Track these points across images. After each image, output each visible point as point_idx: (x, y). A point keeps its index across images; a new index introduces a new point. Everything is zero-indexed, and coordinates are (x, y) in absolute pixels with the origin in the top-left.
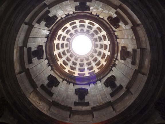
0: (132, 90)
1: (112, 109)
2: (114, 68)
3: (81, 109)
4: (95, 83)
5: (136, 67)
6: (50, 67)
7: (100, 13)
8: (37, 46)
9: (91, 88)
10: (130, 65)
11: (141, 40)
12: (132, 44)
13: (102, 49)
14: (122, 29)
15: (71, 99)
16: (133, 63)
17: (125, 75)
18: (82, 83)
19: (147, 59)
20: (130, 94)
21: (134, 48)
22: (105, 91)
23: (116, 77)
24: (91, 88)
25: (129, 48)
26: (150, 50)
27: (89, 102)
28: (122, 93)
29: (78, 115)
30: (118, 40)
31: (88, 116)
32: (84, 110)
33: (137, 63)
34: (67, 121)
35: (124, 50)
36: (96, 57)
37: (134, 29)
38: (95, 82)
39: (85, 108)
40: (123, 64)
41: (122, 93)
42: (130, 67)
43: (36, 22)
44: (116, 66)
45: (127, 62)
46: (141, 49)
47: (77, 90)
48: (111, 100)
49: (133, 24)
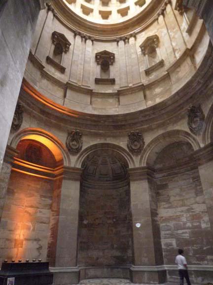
0: (123, 99)
2: (121, 43)
4: (84, 39)
6: (88, 41)
7: (164, 212)
8: (96, 63)
9: (75, 43)
10: (143, 69)
11: (178, 70)
12: (167, 54)
14: (179, 22)
16: (148, 72)
17: (127, 72)
18: (65, 22)
19: (162, 89)
20: (117, 99)
24: (75, 43)
25: (161, 50)
28: (109, 90)
29: (48, 80)
30: (161, 17)
31: (59, 89)
32: (56, 77)
33: (150, 78)
34: (36, 85)
35: (154, 42)
37: (190, 53)
38: (84, 37)
39: (57, 75)
41: (109, 90)
42: (141, 71)
44: (127, 45)
45: (142, 58)
46: (168, 73)
47: (56, 35)
49: (192, 48)
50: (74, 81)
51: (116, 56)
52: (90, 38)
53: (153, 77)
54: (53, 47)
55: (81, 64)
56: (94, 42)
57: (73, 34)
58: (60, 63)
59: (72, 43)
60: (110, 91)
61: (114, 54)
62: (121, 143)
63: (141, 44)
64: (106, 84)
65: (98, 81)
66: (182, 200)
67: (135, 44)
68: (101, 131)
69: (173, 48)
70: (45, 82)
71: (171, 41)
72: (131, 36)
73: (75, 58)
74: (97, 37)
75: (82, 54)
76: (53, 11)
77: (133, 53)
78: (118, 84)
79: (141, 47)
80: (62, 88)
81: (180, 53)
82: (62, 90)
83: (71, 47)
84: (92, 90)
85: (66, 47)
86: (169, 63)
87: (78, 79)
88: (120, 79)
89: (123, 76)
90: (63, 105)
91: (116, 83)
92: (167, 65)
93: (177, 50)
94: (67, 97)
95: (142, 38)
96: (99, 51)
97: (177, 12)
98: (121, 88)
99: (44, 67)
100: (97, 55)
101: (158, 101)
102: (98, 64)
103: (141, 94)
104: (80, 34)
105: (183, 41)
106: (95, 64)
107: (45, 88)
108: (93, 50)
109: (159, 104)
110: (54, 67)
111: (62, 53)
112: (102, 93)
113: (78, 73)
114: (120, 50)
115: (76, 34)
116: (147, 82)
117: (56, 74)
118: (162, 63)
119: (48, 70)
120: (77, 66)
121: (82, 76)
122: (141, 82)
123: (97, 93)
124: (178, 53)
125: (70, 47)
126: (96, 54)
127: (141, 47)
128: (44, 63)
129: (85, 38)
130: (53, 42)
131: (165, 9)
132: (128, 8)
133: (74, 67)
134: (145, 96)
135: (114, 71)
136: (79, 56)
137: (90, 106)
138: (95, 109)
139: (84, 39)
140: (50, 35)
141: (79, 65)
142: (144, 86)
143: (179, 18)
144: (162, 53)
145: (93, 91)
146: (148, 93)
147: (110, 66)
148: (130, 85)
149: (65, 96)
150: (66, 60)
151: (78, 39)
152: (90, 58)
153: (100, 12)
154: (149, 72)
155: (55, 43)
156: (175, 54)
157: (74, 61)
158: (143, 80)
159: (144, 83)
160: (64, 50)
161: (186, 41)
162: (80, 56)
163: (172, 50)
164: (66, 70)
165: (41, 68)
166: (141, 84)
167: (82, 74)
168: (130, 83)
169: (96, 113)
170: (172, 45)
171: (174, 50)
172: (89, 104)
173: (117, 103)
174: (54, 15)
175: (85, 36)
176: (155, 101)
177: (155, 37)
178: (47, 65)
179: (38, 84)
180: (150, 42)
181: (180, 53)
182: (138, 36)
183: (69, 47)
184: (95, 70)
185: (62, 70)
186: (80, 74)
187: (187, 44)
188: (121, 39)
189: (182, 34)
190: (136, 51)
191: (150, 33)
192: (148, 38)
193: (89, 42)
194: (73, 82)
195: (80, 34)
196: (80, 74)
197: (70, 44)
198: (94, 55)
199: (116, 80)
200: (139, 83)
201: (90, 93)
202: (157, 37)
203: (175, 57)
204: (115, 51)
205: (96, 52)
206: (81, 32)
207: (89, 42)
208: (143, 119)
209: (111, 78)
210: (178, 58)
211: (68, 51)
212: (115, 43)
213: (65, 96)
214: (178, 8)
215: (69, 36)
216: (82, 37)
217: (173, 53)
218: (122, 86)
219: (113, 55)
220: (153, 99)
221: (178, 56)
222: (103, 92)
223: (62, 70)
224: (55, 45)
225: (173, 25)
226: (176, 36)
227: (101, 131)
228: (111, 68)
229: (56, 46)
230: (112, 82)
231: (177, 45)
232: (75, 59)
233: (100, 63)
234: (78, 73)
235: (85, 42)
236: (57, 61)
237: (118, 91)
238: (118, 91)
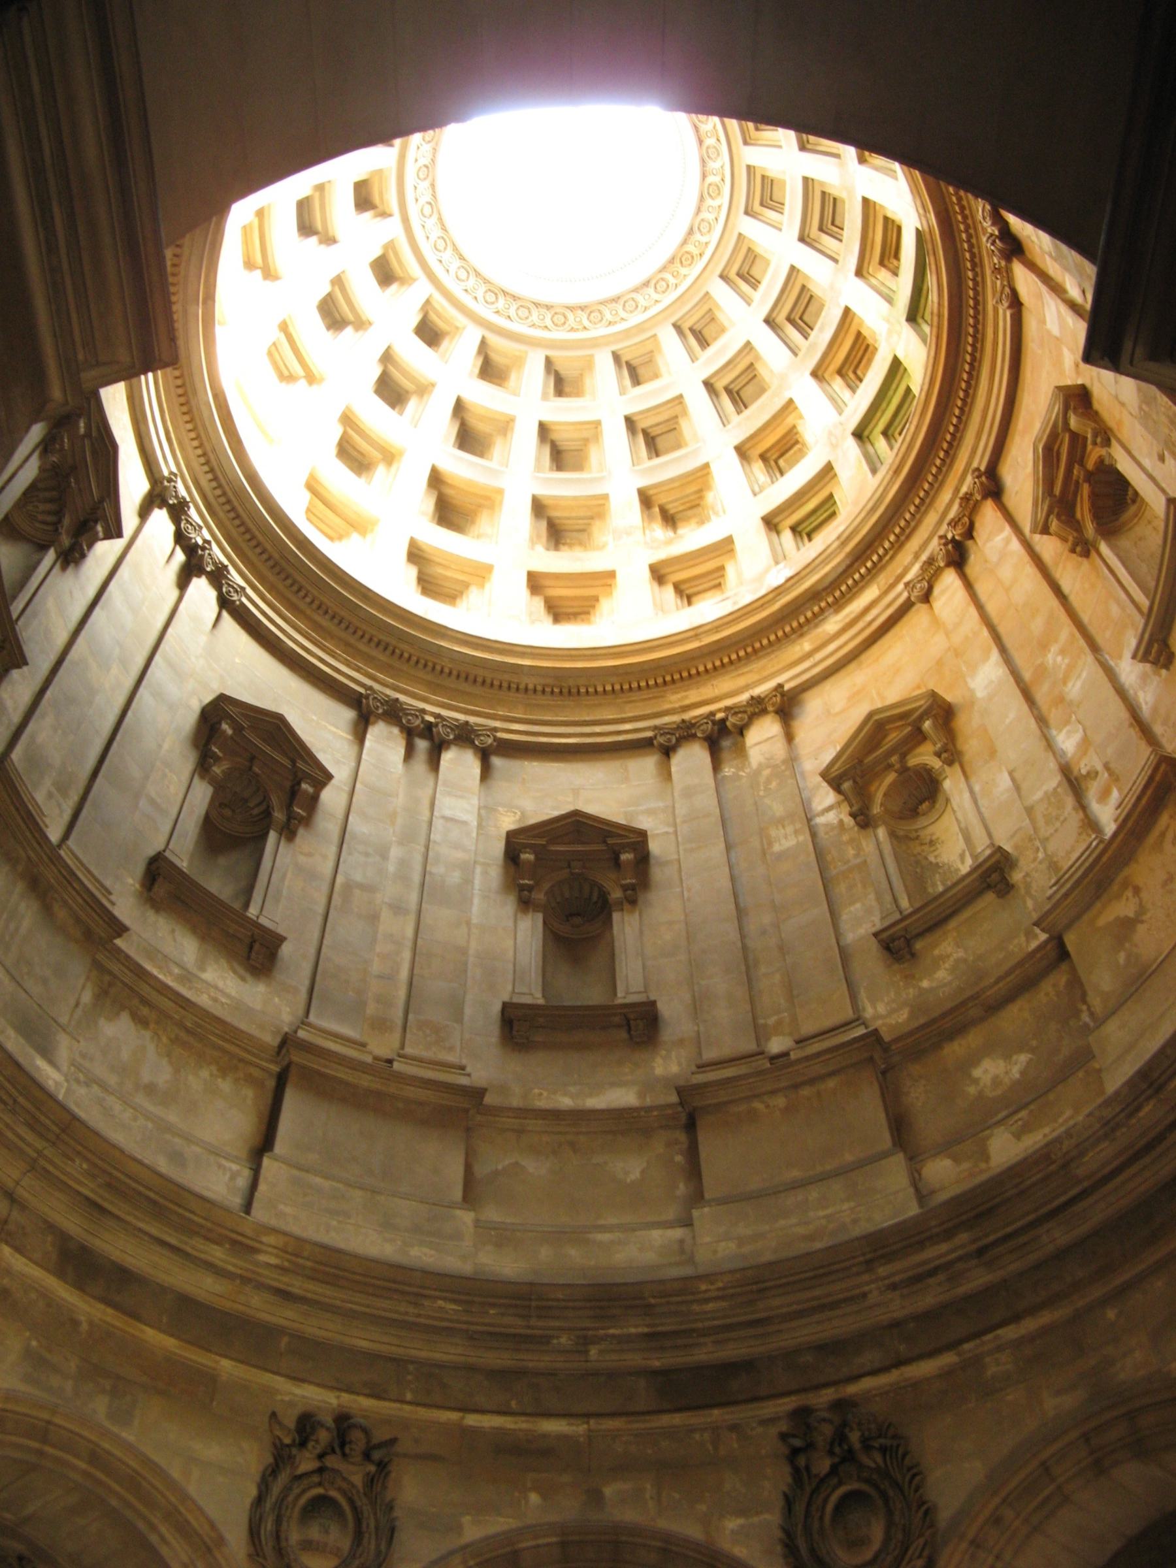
1: (455, 1170)
2: (692, 759)
3: (187, 977)
4: (422, 745)
5: (887, 1008)
6: (449, 757)
10: (862, 919)
12: (1029, 811)
13: (724, 420)
15: (143, 803)
16: (900, 945)
19: (1047, 1130)
21: (1007, 847)
22: (475, 921)
23: (657, 874)
26: (1117, 1093)
27: (281, 939)
29: (141, 1022)
30: (950, 580)
31: (225, 1085)
32: (203, 1000)
33: (925, 984)
36: (597, 424)
38: (428, 731)
39: (220, 985)
40: (805, 837)
42: (850, 937)
43: (802, 454)
48: (484, 1064)
50: (332, 1026)
51: (654, 846)
52: (464, 736)
53: (947, 964)
54: (202, 794)
55: (398, 909)
56: (496, 761)
57: (348, 715)
58: (247, 905)
59: (340, 772)
60: (623, 1097)
61: (643, 834)
62: (732, 1524)
63: (828, 756)
64: (582, 1047)
65: (519, 1026)
66: (1151, 1084)
67: (792, 760)
68: (552, 1426)
69: (1066, 771)
70: (119, 1031)
71: (1042, 721)
72: (757, 708)
73: (355, 868)
74: (516, 731)
75: (406, 838)
76: (217, 577)
77: (780, 822)
78: (681, 1042)
79: (834, 779)
80: (251, 1080)
81: (1115, 795)
82: (249, 1093)
83: (332, 798)
84: (480, 1093)
85: (293, 793)
86: (1053, 866)
87: (371, 1009)
88: (698, 1006)
89: (720, 983)
90: (248, 1207)
91: (667, 1034)
92: (1036, 880)
93: (1093, 775)
94: (279, 1147)
95: (545, 792)
96: (532, 821)
97: (1048, 547)
98: (702, 1067)
99: (120, 929)
100: (515, 844)
101: (1005, 1148)
102: (525, 904)
103: (867, 1109)
104: (393, 713)
105: (1124, 714)
106: (507, 907)
107: (112, 1080)
108: (486, 812)
109: (1015, 1171)
110: (194, 930)
111: (264, 837)
112: (556, 1115)
113: (376, 967)
114: (682, 810)
115: (365, 712)
116: (903, 1015)
117: (209, 975)
118: (995, 874)
119: (153, 953)
120: (374, 918)
121: (402, 994)
122: (858, 1020)
123: (525, 1113)
124: (1104, 795)
125: (326, 795)
126: (511, 836)
127: (834, 779)
128: (125, 903)
129: (429, 740)
130: (203, 766)
131: (969, 533)
132: (726, 546)
133: (346, 929)
134: (900, 1127)
135: (647, 949)
136: (384, 854)
137: (466, 1218)
138: (501, 1237)
139: (422, 745)
140: (188, 718)
141: (386, 915)
142: (885, 1047)
143: (1073, 575)
144: (977, 813)
145: (488, 1099)
146: (918, 1095)
147: (616, 916)
148: (776, 1045)
149: (264, 1144)
150: (292, 879)
151: (385, 744)
152: (467, 869)
153: (535, 583)
154: (909, 943)
155: (217, 770)
156: (1082, 806)
157: (349, 886)
158: (1062, 652)
159: (878, 1023)
160: (279, 815)
161: (1146, 711)
162: (395, 852)
163: (1054, 781)
164: (286, 950)
165: (97, 931)
166: (861, 1031)
167: (404, 974)
168: (777, 1029)
169: (507, 1265)
170: (1050, 745)
171: (1074, 782)
172: (458, 1194)
173: (682, 1189)
174: (224, 603)
175: (429, 726)
176: (985, 1156)
177: (633, 838)
178: (151, 915)
179: (64, 1047)
180: (893, 737)
181: (1115, 795)
182: (814, 706)
183: (315, 798)
184: (504, 943)
185: (257, 951)
186: (389, 978)
187: (1158, 729)
188: (685, 733)
189: (1111, 674)
190: (805, 806)
191: (892, 677)
192: (576, 813)
193: (460, 764)
194: (337, 1036)
195: (393, 713)
196: (389, 978)
197: (323, 778)
198: (499, 847)
199: (664, 1008)
200: (846, 1025)
201: (459, 1110)
202: (942, 713)
203: (1091, 824)
204: (651, 812)
205: (509, 823)
206: (402, 698)
207: (460, 764)
208: (898, 1307)
209: (623, 997)
210: (1110, 828)
211: (307, 821)
212: (648, 764)
213: (264, 1144)
214: (1054, 524)
215: (319, 724)
216: (410, 734)
217: (1070, 802)
218: (709, 1055)
219: (638, 840)
220: (966, 1139)
221: (1107, 815)
222: (566, 1102)
223: (257, 951)
224: (213, 781)
225: (1037, 625)
226: (1074, 689)
227: (552, 1426)
228: (625, 927)
229: (219, 787)
230: (640, 1025)
231: (1085, 743)
232: (358, 877)
233: (539, 896)
234: (376, 967)
235: (434, 763)
236: (218, 884)
237: (680, 1091)
238: (680, 1091)
